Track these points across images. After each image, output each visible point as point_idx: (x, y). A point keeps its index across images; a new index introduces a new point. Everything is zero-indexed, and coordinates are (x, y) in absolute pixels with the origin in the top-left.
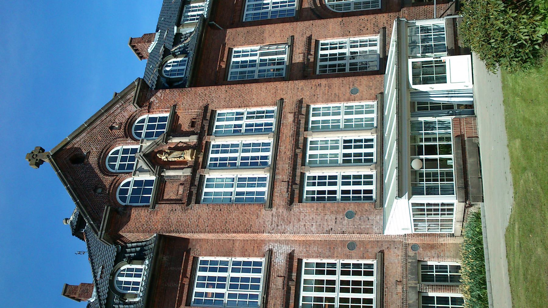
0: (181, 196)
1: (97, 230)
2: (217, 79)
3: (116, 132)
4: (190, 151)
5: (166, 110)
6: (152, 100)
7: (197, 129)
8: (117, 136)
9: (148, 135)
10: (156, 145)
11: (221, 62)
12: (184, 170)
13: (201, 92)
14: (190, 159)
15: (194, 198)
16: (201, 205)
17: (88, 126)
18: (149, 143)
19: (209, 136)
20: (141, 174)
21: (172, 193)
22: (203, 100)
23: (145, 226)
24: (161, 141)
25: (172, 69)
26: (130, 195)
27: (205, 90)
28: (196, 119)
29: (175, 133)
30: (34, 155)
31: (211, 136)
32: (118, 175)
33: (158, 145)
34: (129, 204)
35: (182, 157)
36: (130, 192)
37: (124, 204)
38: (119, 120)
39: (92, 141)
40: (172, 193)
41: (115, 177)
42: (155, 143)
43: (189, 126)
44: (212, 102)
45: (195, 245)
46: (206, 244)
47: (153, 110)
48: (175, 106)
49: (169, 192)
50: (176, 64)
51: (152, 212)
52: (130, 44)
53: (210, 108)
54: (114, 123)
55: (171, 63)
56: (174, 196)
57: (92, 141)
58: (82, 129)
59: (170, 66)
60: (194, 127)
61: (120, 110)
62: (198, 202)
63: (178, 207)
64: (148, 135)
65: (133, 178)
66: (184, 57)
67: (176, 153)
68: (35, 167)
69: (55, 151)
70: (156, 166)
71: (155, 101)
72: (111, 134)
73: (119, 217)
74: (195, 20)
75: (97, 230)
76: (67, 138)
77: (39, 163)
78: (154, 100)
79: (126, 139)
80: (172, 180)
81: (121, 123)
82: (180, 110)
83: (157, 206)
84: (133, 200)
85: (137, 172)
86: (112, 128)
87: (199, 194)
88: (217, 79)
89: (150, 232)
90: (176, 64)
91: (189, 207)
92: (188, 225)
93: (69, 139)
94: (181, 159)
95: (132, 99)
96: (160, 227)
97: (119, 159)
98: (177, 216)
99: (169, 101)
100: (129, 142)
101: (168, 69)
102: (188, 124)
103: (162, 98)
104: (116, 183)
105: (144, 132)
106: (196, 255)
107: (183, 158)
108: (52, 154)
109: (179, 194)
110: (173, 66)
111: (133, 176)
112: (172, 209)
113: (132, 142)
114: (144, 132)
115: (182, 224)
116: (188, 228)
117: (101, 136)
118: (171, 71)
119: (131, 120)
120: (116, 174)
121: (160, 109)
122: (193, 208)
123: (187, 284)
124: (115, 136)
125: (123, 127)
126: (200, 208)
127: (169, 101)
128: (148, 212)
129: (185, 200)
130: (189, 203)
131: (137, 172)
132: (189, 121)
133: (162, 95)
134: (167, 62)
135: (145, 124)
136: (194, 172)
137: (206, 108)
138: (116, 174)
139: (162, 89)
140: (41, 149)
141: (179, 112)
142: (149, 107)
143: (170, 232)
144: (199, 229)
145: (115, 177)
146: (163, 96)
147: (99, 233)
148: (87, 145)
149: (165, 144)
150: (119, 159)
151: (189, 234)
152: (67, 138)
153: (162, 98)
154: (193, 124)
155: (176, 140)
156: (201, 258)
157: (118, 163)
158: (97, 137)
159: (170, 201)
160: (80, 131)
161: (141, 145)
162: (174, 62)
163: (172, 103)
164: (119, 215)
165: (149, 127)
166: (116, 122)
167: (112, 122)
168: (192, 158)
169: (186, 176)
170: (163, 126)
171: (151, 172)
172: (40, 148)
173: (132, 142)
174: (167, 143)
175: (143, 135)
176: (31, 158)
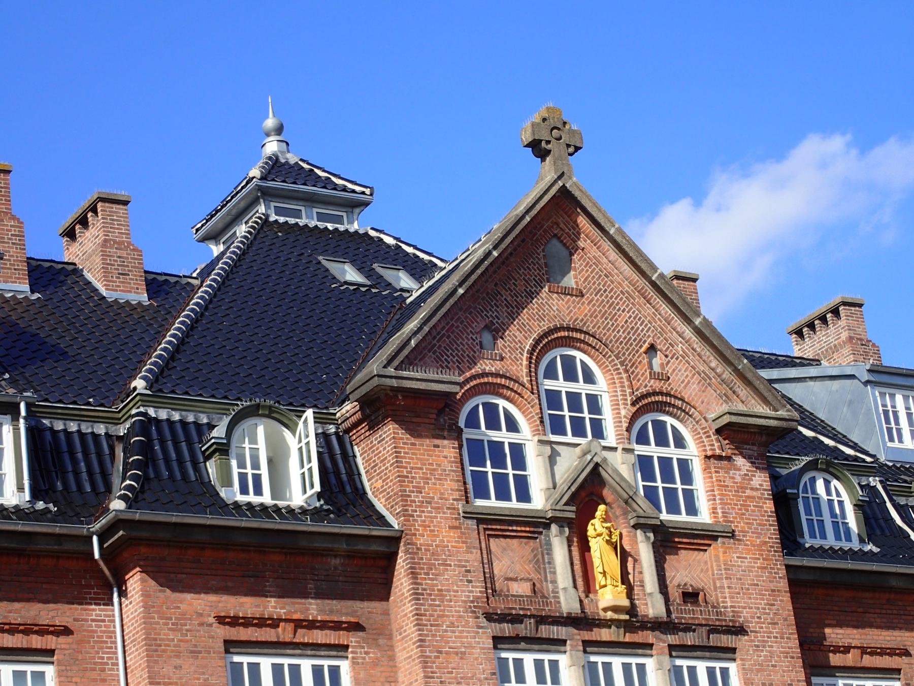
0: (505, 590)
1: (396, 362)
2: (812, 647)
3: (642, 370)
4: (626, 603)
5: (719, 511)
6: (740, 461)
7: (685, 613)
8: (633, 372)
9: (645, 463)
10: (626, 496)
11: (860, 651)
12: (572, 590)
13: (778, 610)
14: (602, 604)
15: (507, 629)
16: (492, 656)
17: (653, 284)
18: (625, 471)
19: (666, 650)
20: (544, 461)
21: (509, 563)
22: (759, 618)
23: (417, 497)
24: (641, 513)
25: (821, 500)
26: (486, 439)
27: (786, 620)
28: (706, 602)
29: (661, 546)
30: (559, 129)
31: (668, 657)
32: (533, 393)
33: (626, 502)
34: (465, 436)
35: (606, 579)
36: (495, 436)
37: (462, 423)
38: (674, 370)
39: (612, 297)
40: (509, 563)
41: (528, 385)
42: (631, 494)
43: (685, 585)
44: (758, 646)
45: (378, 646)
46: (387, 677)
47: (713, 470)
48: (732, 535)
49: (511, 554)
50: (838, 511)
51: (456, 512)
52: (844, 304)
53: (741, 642)
54: (666, 356)
55: (838, 495)
56: (501, 570)
57: (612, 297)
58: (643, 266)
59: (828, 493)
60: (684, 602)
61: (702, 368)
62: (498, 641)
63: (477, 589)
64: (645, 463)
65: (530, 438)
66: (859, 535)
67: (614, 563)
68: (527, 137)
69: (577, 194)
70: (574, 508)
71: (737, 472)
72: (637, 351)
73: (431, 416)
74: (886, 424)
75: (396, 362)
76: (617, 226)
77: (538, 149)
78: (739, 470)
79: (629, 402)
80: (540, 556)
81: (669, 378)
82: (725, 552)
83: (472, 524)
84: (476, 448)
85: (547, 450)
86: (652, 349)
87: (513, 642)
88: (812, 647)
89: (406, 515)
90: (838, 511)
91: (483, 621)
92: (437, 625)
93: (612, 232)
94: (599, 579)
95: (741, 408)
96: (422, 542)
97: (572, 387)
98: (455, 588)
99: (743, 514)
100: (623, 412)
101: (820, 485)
102: (690, 582)
103: (748, 492)
104: (508, 388)
105: (652, 450)
106: (352, 652)
107: (603, 583)
108: (568, 185)
109: (510, 583)
110: (830, 502)
111: (536, 438)
112: (469, 571)
113: (623, 420)
114: (652, 450)
115: (439, 606)
116: (431, 625)
117: (626, 321)
118: (817, 500)
119: (681, 408)
120: (535, 387)
121: (717, 489)
122: (480, 630)
123: (278, 637)
124: (631, 367)
125: (656, 385)
126: (485, 654)
127: (743, 514)
128: (454, 500)
129: (499, 606)
130: (489, 617)
131: (547, 450)
132: (698, 584)
133: (757, 489)
134: (838, 478)
135: (672, 452)
136: (572, 621)
137: (740, 630)
138: (535, 388)
139: (772, 490)
140: (577, 149)
141: (717, 548)
142: (720, 458)
143: (413, 574)
144: (430, 657)
145: (528, 385)
146: (754, 493)
147: (391, 371)
148: (600, 284)
149: (632, 522)
150: (572, 387)
151: (410, 629)
152: (617, 226)
153: (748, 492)
154: (691, 596)
155: (645, 552)
156: (345, 666)
157: (561, 385)
158: (623, 311)
159: (487, 561)
160: (638, 261)
161: (616, 448)
162: (841, 503)
163: (739, 526)
164: (434, 416)
165: (665, 463)
166: (669, 362)
167: (666, 351)
168: (605, 610)
169: (558, 598)
170: (673, 508)
171: (557, 496)
172: (578, 145)
173: (623, 420)
174: (636, 527)
175: (641, 450)
176: (551, 123)
